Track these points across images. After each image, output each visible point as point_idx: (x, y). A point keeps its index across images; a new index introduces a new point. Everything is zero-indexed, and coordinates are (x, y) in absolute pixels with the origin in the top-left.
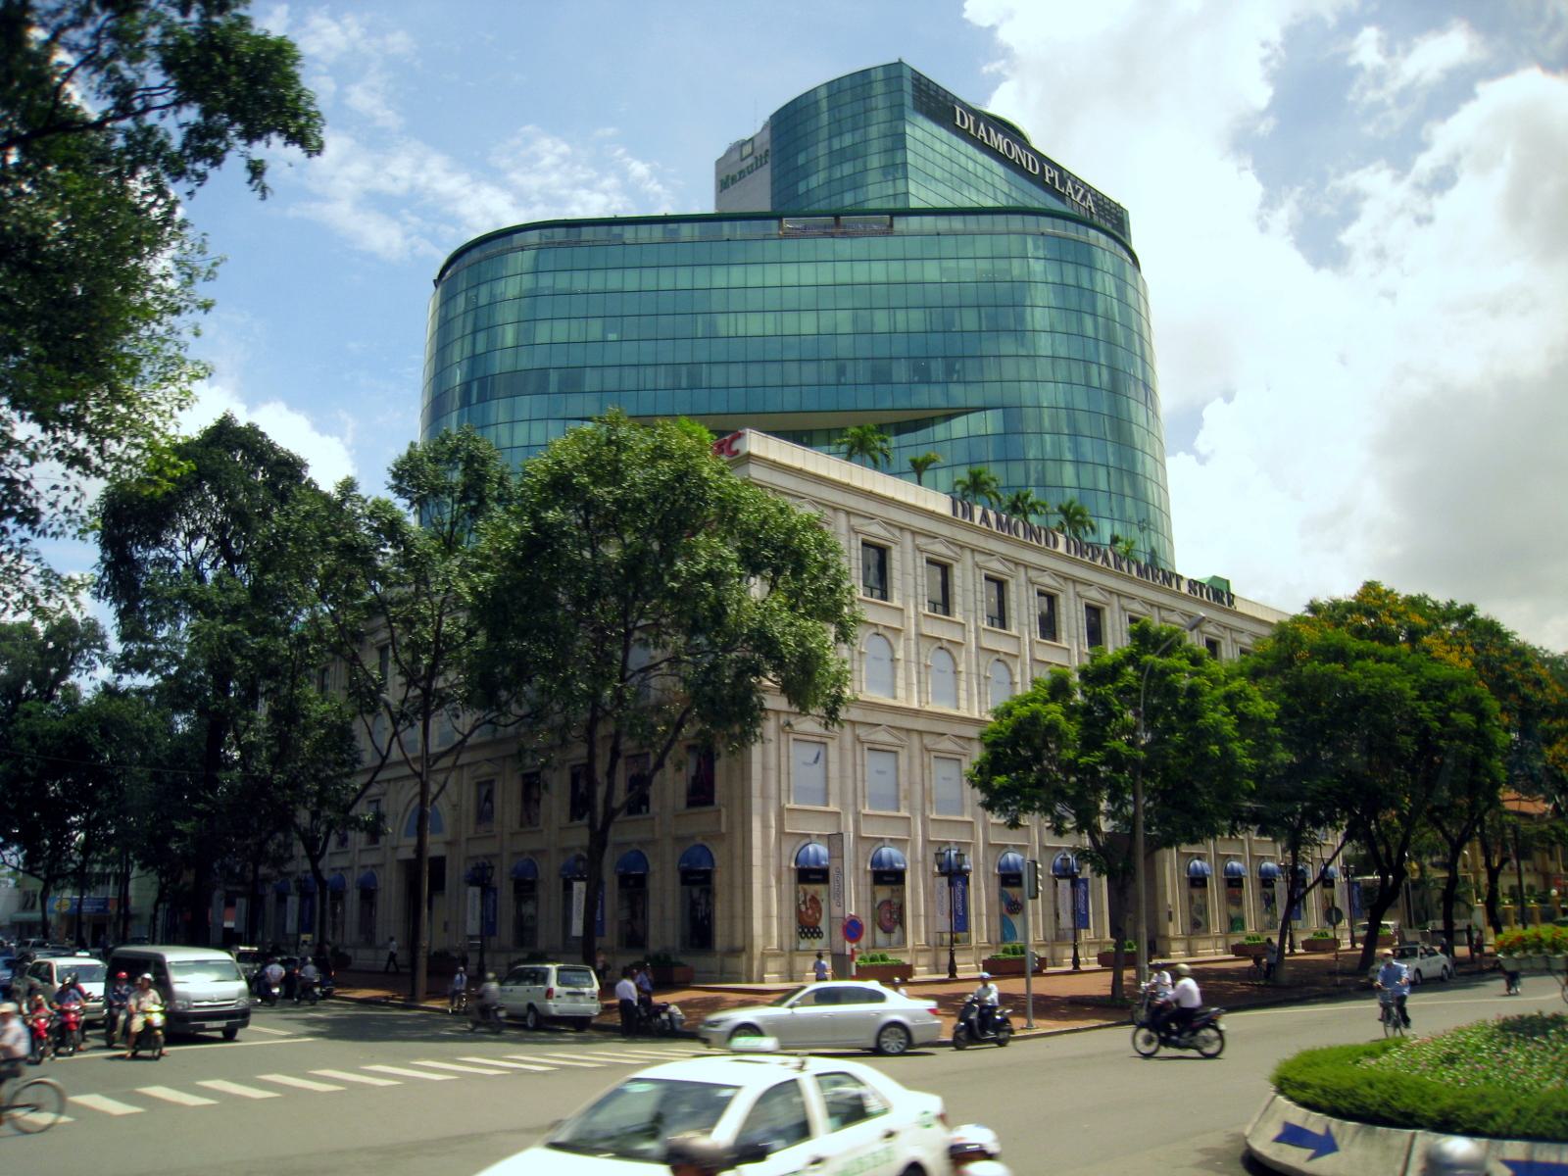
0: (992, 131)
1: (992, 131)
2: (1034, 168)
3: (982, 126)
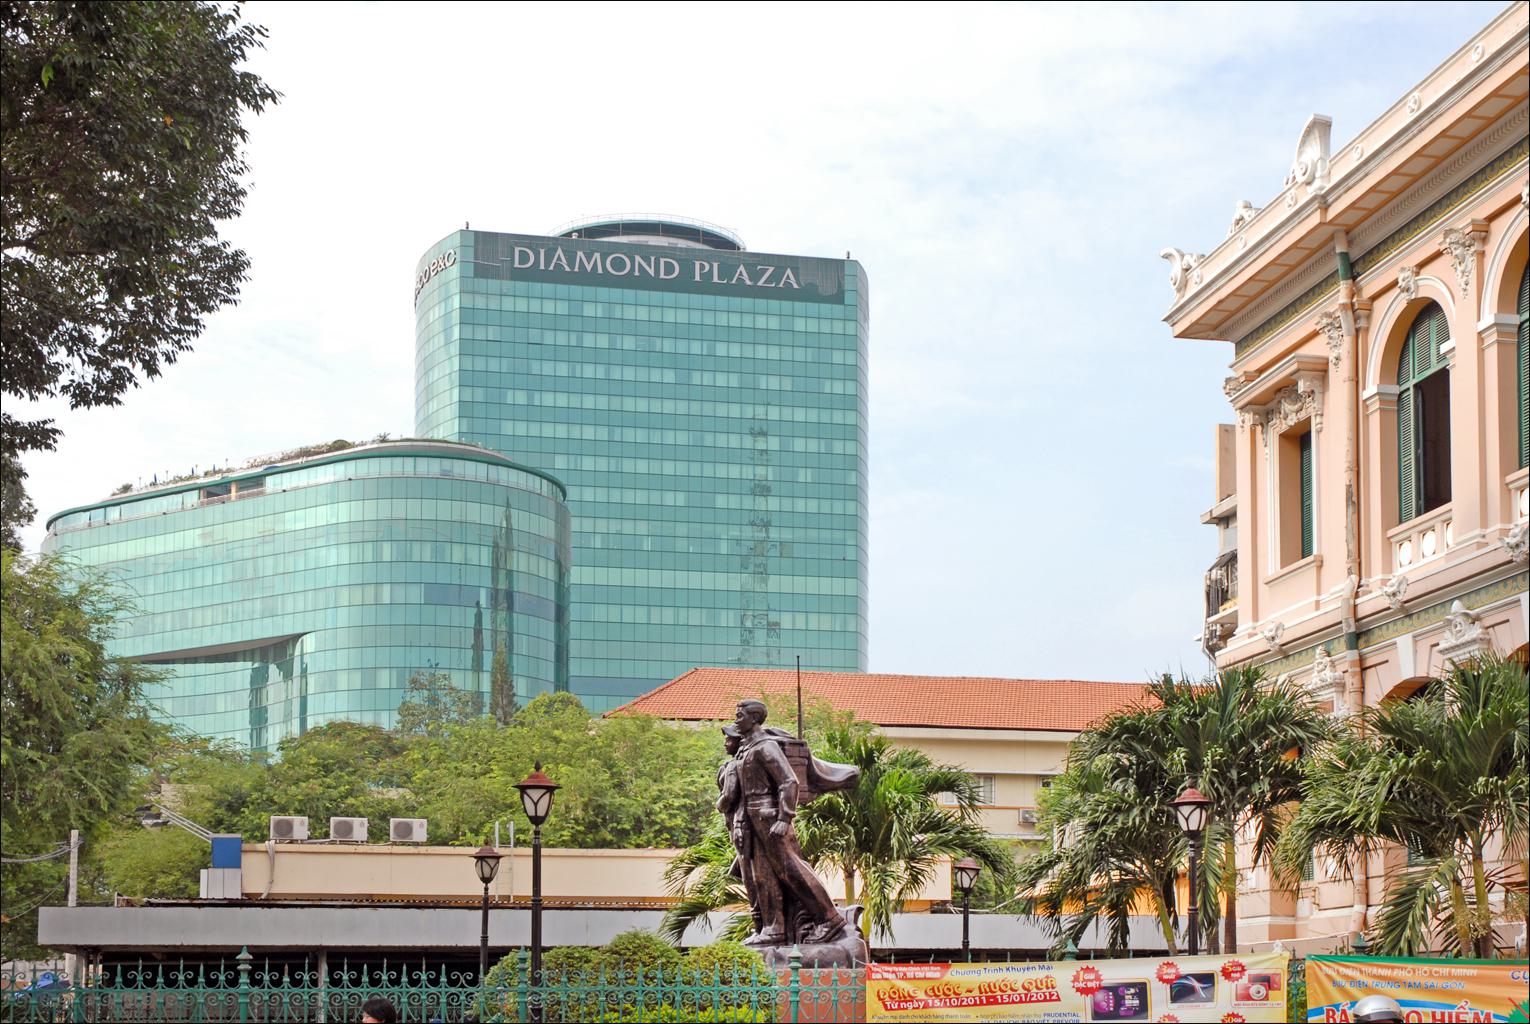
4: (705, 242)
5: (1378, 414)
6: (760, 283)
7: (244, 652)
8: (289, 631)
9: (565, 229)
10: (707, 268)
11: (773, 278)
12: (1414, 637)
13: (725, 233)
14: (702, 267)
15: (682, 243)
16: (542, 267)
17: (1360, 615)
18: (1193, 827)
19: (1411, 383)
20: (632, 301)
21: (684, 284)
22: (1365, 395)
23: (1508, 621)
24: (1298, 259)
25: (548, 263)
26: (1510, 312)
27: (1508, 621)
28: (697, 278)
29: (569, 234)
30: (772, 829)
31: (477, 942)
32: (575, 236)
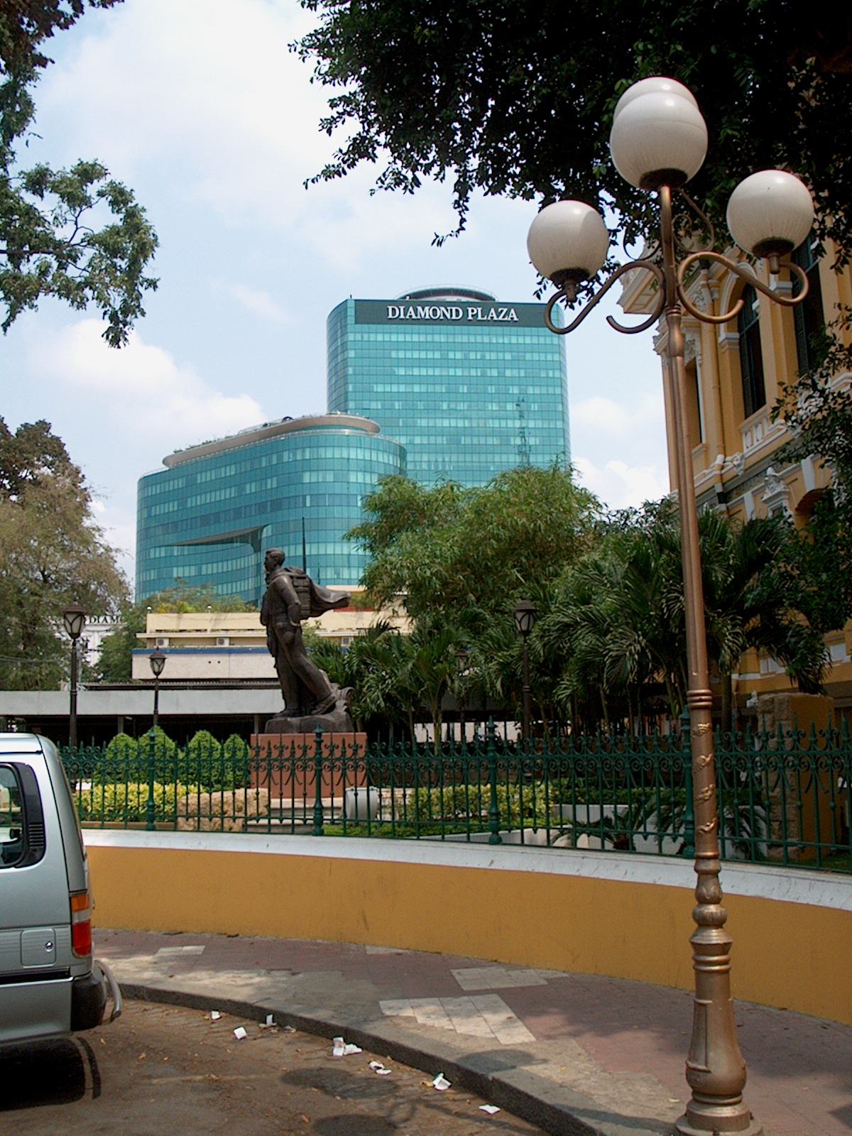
0: (420, 308)
1: (420, 308)
2: (457, 316)
3: (411, 309)
4: (476, 298)
5: (727, 354)
6: (500, 318)
7: (217, 515)
8: (258, 524)
9: (402, 295)
10: (475, 312)
11: (507, 313)
12: (753, 493)
13: (488, 293)
14: (473, 311)
15: (464, 299)
16: (402, 316)
17: (724, 481)
18: (524, 628)
19: (744, 332)
20: (431, 331)
21: (464, 322)
22: (720, 339)
23: (796, 479)
24: (764, 295)
25: (405, 315)
26: (786, 281)
27: (796, 479)
28: (470, 318)
29: (405, 297)
30: (758, 617)
31: (67, 712)
32: (408, 298)
